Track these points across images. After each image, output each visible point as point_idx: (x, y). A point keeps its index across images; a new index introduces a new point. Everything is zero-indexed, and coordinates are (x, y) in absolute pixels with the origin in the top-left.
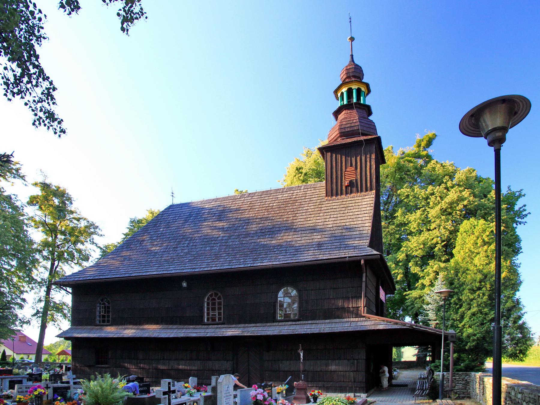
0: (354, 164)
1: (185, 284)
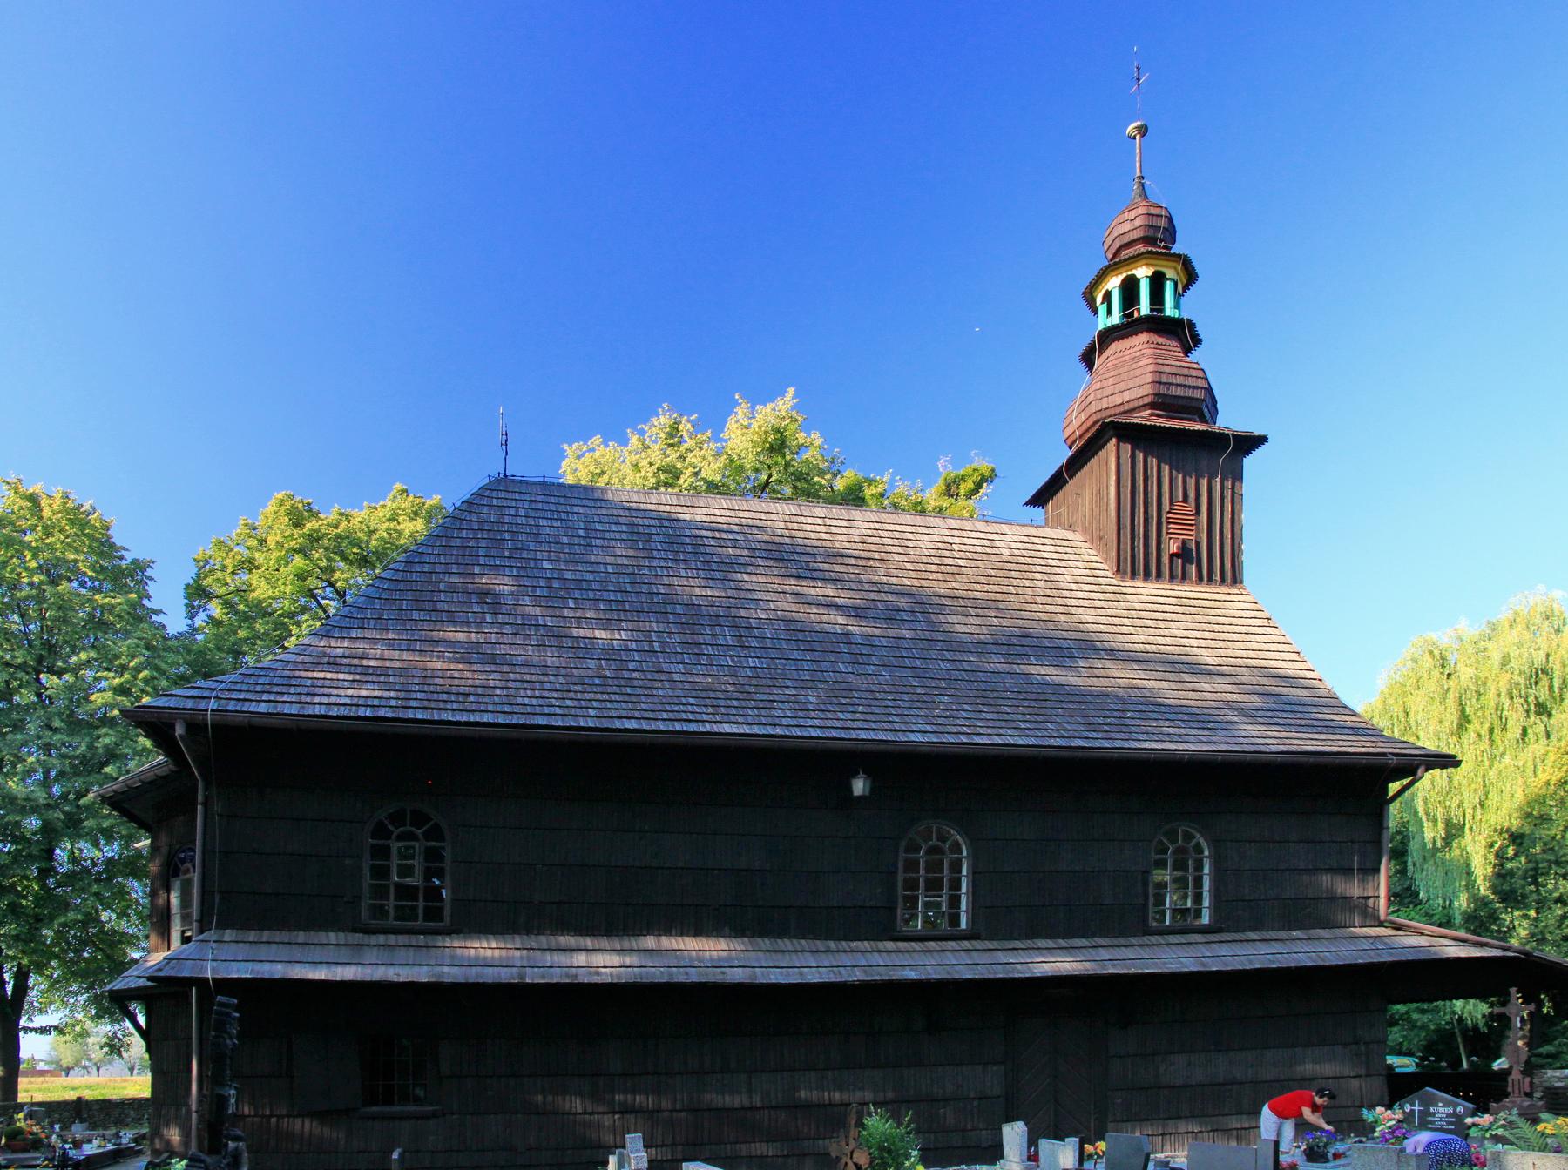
0: (1192, 495)
1: (859, 786)
